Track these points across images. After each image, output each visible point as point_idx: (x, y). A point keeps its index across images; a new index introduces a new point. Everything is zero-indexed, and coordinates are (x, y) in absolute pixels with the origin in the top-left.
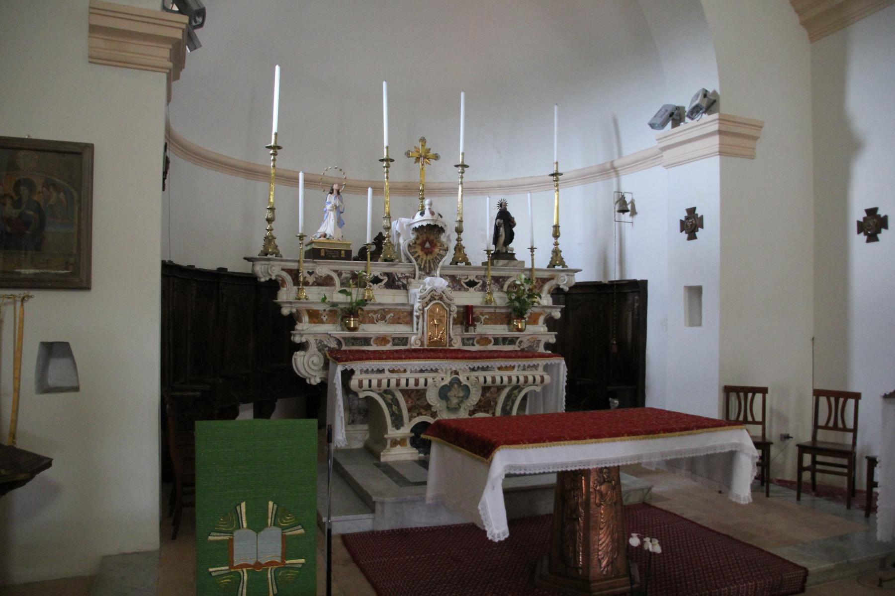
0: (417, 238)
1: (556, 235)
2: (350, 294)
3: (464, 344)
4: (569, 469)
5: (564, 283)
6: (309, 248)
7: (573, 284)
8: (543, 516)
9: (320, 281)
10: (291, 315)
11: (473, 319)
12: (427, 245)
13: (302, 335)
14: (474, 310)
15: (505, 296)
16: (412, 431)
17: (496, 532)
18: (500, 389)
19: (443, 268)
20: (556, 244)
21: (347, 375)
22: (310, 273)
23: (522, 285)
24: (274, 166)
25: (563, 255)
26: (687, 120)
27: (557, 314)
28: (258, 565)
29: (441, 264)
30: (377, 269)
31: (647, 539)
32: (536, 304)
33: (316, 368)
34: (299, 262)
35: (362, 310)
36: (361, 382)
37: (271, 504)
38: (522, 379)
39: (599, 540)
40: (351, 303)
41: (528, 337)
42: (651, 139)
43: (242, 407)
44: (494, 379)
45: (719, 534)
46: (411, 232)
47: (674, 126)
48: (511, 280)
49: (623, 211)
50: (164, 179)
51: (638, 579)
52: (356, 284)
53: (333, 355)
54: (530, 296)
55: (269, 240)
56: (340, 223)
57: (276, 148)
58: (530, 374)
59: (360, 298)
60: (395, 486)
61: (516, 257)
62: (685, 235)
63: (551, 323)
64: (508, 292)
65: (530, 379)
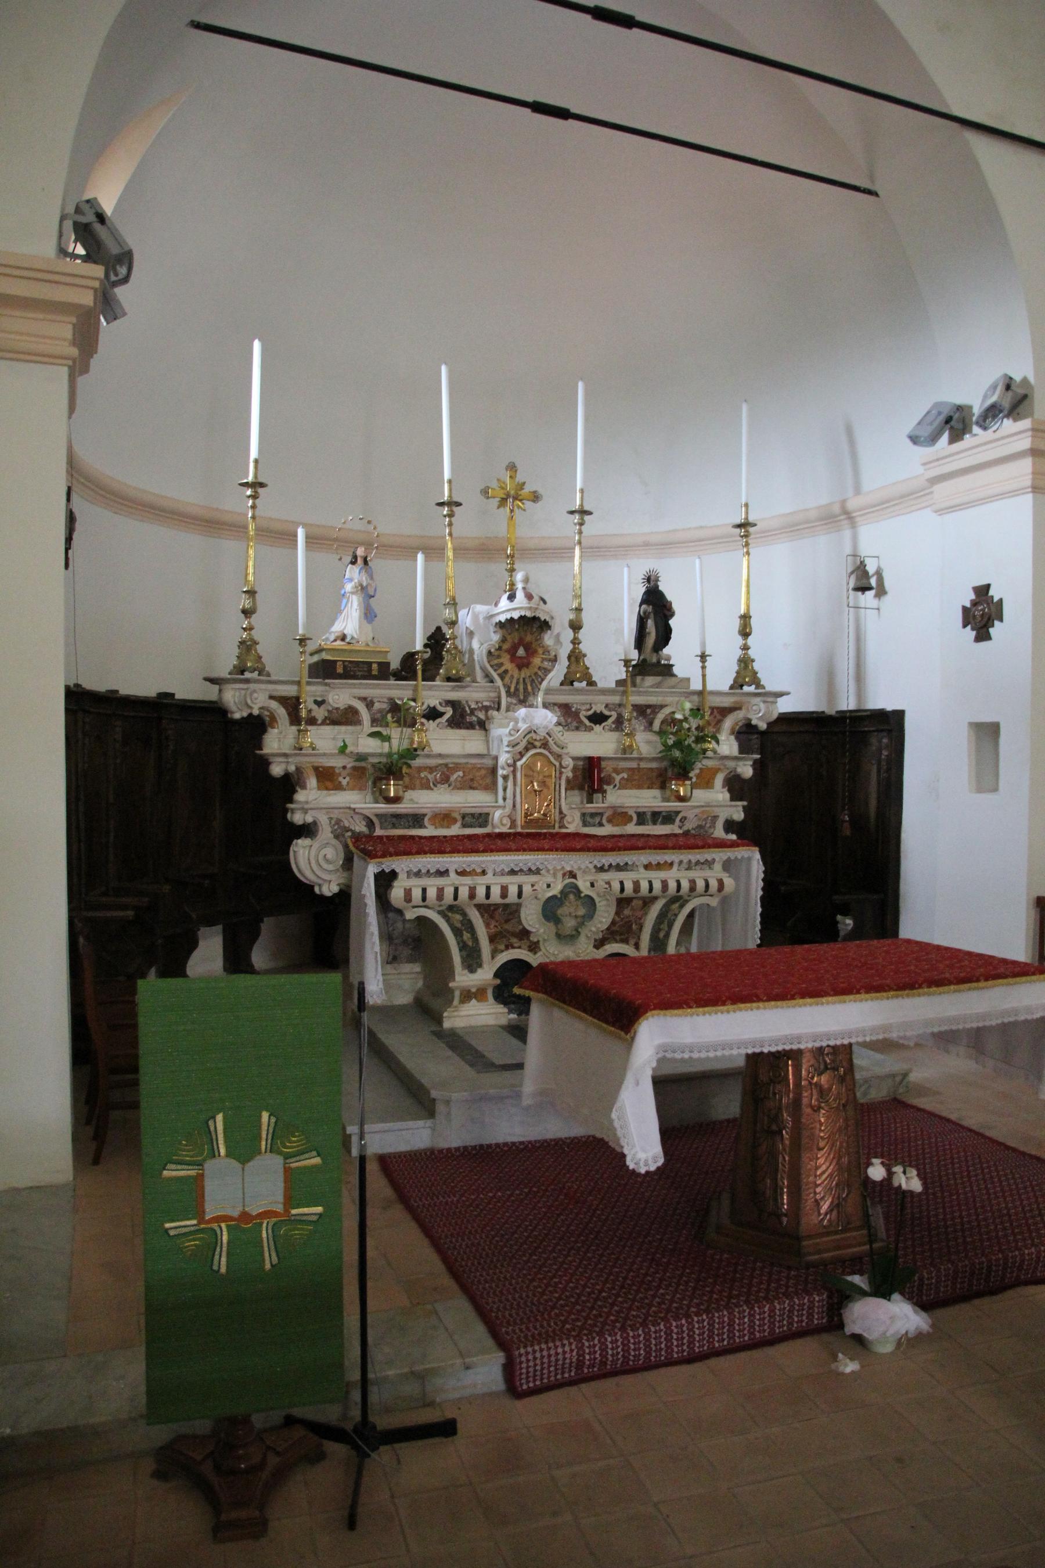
0: (504, 640)
1: (745, 632)
2: (387, 739)
3: (585, 824)
4: (766, 1051)
5: (760, 715)
6: (316, 658)
7: (775, 716)
8: (721, 1122)
9: (335, 716)
10: (287, 776)
11: (600, 780)
12: (521, 652)
13: (305, 811)
14: (603, 764)
15: (655, 738)
16: (496, 975)
17: (642, 1156)
18: (648, 902)
19: (548, 691)
20: (745, 648)
21: (385, 880)
22: (319, 704)
23: (686, 719)
24: (253, 517)
25: (756, 666)
26: (976, 429)
27: (747, 771)
28: (245, 1216)
29: (545, 684)
30: (435, 694)
31: (898, 1169)
32: (709, 754)
33: (331, 867)
34: (299, 683)
35: (409, 766)
36: (408, 893)
37: (265, 1116)
38: (685, 885)
39: (817, 1168)
40: (389, 755)
41: (697, 811)
42: (912, 463)
43: (203, 931)
44: (637, 885)
45: (1023, 1154)
46: (492, 629)
47: (953, 440)
48: (667, 711)
49: (863, 589)
50: (67, 550)
51: (882, 1233)
52: (398, 722)
53: (360, 846)
54: (700, 740)
55: (247, 646)
56: (369, 615)
57: (257, 485)
58: (699, 876)
59: (405, 745)
60: (470, 1072)
61: (676, 670)
62: (970, 633)
63: (736, 786)
64: (661, 733)
65: (700, 885)
